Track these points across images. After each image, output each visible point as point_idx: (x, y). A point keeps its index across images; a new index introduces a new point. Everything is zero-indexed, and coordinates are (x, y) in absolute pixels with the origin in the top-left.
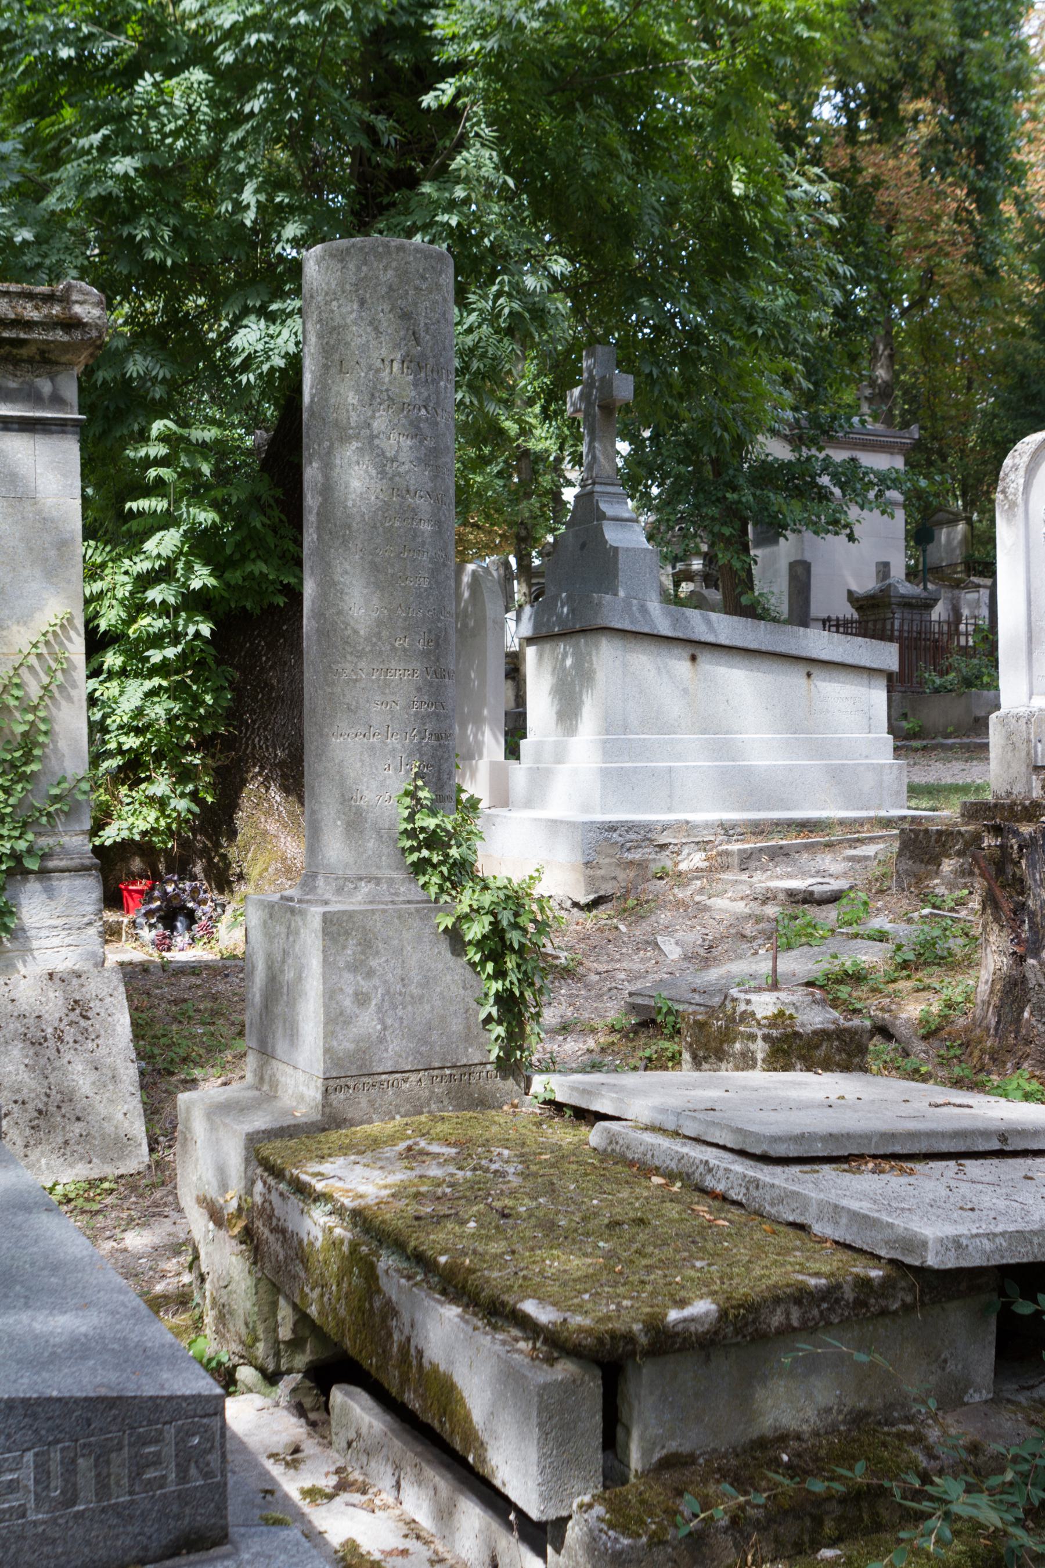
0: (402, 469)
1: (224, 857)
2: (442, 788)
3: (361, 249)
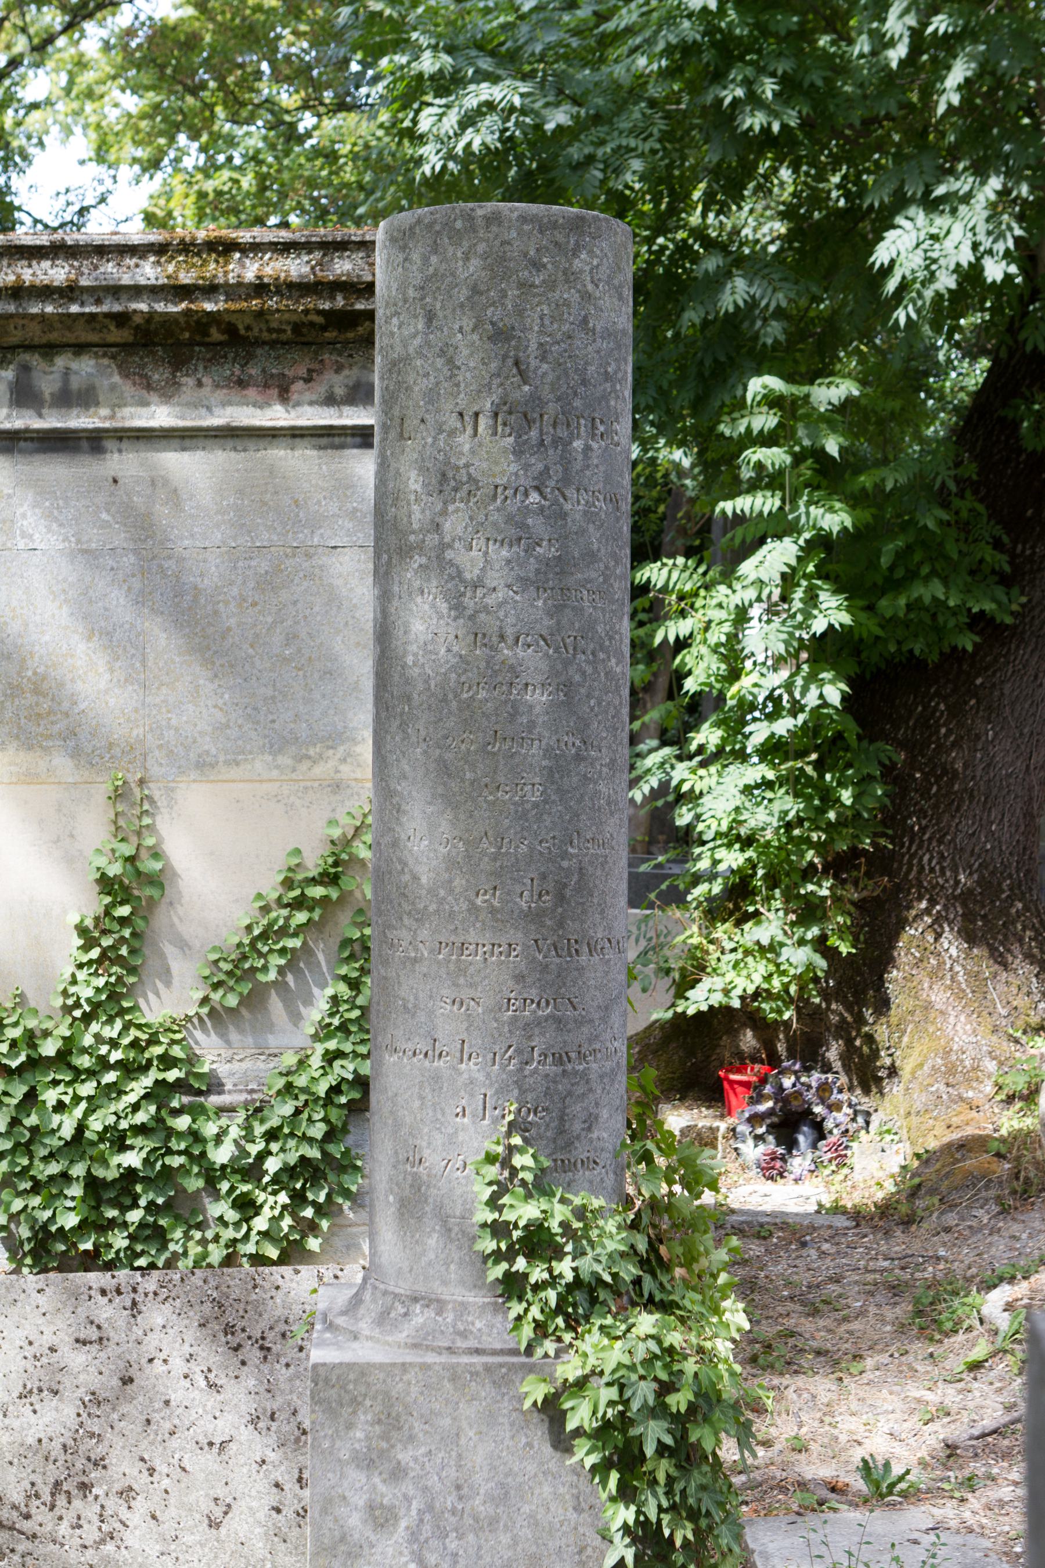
0: (490, 600)
1: (870, 1039)
2: (569, 1145)
3: (430, 226)
